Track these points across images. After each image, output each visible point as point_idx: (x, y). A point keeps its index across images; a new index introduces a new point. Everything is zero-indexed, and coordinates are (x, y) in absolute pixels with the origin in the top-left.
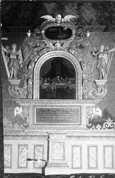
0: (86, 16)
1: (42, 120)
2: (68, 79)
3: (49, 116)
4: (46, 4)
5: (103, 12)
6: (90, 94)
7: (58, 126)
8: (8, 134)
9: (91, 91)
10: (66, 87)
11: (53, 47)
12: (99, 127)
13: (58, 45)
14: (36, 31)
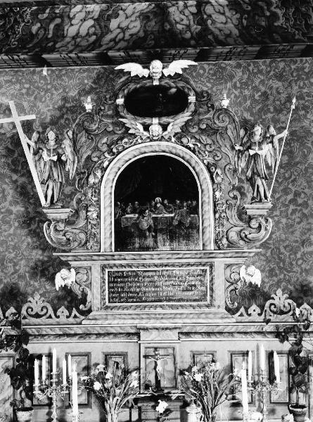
0: (216, 28)
1: (123, 298)
2: (182, 203)
3: (139, 287)
4: (127, 4)
5: (254, 17)
6: (233, 235)
7: (159, 310)
8: (44, 333)
9: (235, 229)
10: (175, 223)
11: (146, 133)
12: (254, 311)
13: (156, 129)
14: (106, 100)
